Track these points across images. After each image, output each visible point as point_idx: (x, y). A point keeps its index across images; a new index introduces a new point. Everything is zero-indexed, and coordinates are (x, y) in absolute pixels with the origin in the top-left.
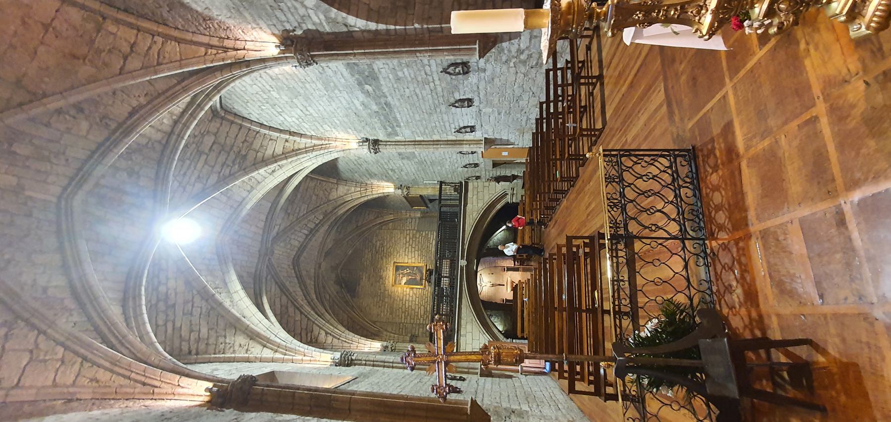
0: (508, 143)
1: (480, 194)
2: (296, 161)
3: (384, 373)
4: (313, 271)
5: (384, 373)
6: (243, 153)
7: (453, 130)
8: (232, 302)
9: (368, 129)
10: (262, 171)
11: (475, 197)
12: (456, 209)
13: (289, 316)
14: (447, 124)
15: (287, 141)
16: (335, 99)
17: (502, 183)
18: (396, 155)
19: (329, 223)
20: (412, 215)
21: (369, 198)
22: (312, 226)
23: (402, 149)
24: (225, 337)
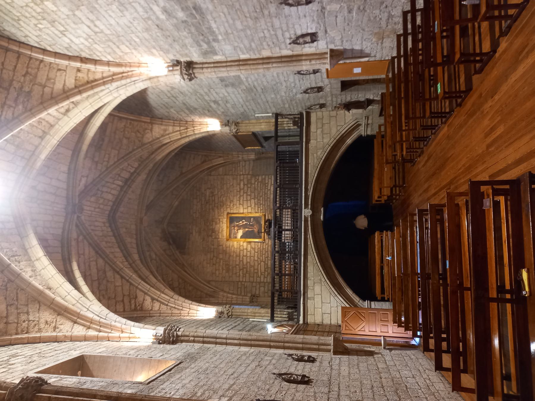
0: (361, 54)
1: (326, 127)
2: (94, 95)
3: (215, 353)
4: (133, 227)
5: (215, 353)
6: (27, 89)
7: (288, 41)
8: (33, 271)
9: (178, 47)
10: (52, 111)
11: (319, 131)
12: (297, 148)
13: (108, 281)
14: (279, 33)
15: (79, 70)
16: (128, 6)
17: (353, 111)
18: (217, 81)
19: (146, 171)
20: (245, 157)
21: (191, 138)
22: (126, 175)
23: (224, 73)
24: (28, 313)
